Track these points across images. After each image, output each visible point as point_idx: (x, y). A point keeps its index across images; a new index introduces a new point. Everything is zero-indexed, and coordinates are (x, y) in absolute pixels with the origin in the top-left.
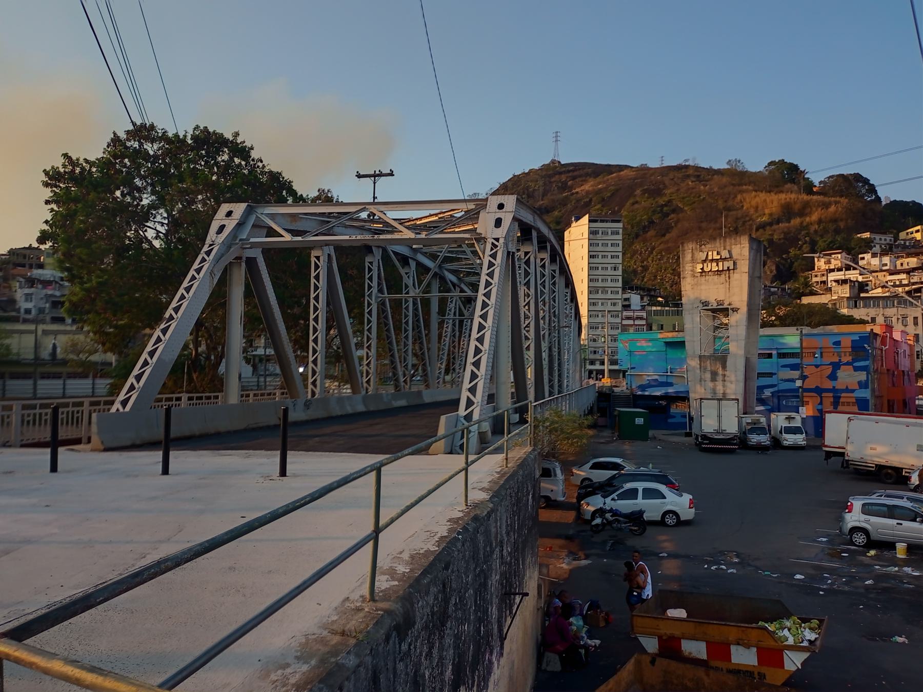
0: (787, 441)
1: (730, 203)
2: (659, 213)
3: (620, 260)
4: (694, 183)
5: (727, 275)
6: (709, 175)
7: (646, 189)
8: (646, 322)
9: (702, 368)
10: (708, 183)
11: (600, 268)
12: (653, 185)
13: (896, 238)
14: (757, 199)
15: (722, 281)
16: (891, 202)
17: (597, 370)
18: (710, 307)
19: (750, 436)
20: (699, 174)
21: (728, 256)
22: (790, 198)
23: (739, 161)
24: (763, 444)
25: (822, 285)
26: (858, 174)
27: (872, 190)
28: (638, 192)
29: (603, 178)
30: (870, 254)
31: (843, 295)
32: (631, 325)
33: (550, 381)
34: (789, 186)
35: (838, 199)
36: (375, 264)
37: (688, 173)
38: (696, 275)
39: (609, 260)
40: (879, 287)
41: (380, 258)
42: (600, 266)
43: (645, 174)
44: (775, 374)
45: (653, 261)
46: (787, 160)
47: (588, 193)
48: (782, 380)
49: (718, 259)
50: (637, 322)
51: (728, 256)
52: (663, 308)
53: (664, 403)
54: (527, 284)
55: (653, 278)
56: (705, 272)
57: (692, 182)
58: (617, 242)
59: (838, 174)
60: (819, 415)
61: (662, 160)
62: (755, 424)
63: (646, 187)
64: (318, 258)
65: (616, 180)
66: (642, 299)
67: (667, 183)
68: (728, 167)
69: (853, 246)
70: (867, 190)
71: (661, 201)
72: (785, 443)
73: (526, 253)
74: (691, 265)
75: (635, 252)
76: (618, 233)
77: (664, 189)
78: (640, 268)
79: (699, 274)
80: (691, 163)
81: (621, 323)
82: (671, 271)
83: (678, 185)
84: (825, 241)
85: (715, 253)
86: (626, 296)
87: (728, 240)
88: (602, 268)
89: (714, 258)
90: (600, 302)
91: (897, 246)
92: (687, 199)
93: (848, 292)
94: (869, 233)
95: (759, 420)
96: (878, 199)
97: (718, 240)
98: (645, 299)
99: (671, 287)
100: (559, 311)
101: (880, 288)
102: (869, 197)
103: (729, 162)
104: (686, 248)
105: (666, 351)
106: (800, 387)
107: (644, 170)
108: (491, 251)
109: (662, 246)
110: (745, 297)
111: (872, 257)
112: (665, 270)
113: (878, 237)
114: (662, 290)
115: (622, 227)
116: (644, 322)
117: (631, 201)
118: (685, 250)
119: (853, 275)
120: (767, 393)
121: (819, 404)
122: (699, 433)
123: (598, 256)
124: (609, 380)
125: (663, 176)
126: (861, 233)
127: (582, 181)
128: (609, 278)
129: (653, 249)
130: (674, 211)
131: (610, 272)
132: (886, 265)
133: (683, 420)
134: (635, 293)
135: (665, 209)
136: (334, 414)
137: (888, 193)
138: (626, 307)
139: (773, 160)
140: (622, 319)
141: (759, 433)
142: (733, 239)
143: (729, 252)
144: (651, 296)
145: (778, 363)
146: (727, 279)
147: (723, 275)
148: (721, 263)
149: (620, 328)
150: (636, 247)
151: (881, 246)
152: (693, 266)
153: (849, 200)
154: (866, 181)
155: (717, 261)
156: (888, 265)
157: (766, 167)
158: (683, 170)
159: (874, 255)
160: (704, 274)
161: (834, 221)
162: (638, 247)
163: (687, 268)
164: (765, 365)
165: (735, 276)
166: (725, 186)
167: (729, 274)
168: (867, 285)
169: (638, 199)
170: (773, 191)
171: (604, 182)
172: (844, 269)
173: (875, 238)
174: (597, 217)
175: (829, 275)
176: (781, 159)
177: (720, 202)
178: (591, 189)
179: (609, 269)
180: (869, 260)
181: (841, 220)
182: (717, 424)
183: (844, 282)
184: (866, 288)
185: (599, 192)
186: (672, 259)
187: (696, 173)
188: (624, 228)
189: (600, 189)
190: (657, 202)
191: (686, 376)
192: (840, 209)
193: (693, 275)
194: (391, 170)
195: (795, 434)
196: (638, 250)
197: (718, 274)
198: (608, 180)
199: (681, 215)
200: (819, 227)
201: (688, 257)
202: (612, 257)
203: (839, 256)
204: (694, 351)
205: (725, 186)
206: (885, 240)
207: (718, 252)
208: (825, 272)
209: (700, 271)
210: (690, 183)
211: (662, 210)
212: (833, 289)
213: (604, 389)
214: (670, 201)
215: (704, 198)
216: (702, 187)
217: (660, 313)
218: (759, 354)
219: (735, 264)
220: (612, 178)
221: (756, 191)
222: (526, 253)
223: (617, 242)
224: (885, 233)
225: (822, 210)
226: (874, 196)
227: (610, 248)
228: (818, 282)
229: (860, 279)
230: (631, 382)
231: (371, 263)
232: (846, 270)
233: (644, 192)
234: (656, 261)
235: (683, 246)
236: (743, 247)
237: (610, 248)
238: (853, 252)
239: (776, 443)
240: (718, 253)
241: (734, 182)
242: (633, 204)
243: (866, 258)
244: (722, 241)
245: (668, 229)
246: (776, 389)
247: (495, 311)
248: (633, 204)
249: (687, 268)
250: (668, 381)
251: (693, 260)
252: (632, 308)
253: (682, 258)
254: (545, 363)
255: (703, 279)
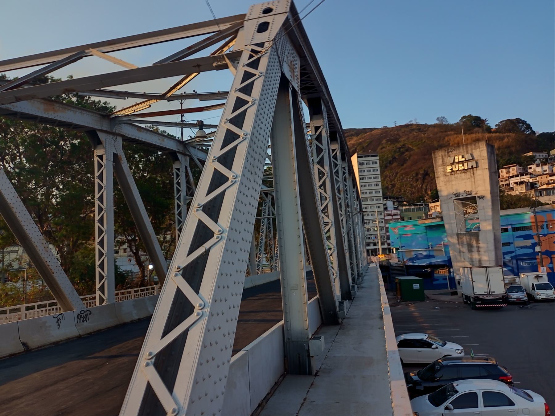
0: (540, 295)
1: (441, 143)
2: (398, 152)
3: (379, 180)
4: (417, 133)
5: (472, 172)
6: (426, 128)
7: (389, 139)
8: (400, 216)
9: (460, 243)
10: (426, 132)
11: (367, 186)
12: (393, 137)
13: (549, 155)
14: (458, 139)
15: (468, 177)
16: (540, 134)
17: (372, 249)
18: (461, 197)
19: (511, 294)
20: (419, 128)
21: (471, 158)
22: (479, 136)
23: (444, 117)
24: (521, 299)
25: (506, 186)
26: (518, 118)
27: (529, 127)
28: (384, 141)
29: (362, 135)
30: (535, 165)
31: (521, 191)
32: (391, 220)
33: (351, 263)
34: (476, 129)
35: (508, 134)
36: (183, 170)
37: (413, 128)
38: (447, 174)
39: (372, 180)
40: (544, 185)
41: (188, 165)
42: (367, 184)
43: (387, 131)
44: (512, 243)
45: (397, 181)
46: (474, 115)
47: (354, 145)
48: (518, 247)
49: (463, 161)
50: (394, 217)
51: (471, 158)
52: (410, 207)
53: (429, 270)
54: (321, 163)
55: (399, 191)
56: (454, 171)
57: (416, 132)
58: (377, 168)
59: (506, 119)
60: (551, 272)
61: (395, 124)
62: (511, 284)
63: (388, 138)
64: (101, 157)
65: (370, 136)
66: (394, 204)
67: (401, 134)
68: (437, 122)
69: (522, 161)
70: (525, 128)
71: (399, 145)
72: (539, 297)
73: (317, 129)
74: (442, 167)
75: (386, 176)
76: (376, 163)
77: (399, 138)
78: (390, 186)
79: (450, 174)
80: (414, 122)
81: (384, 218)
82: (410, 186)
83: (408, 135)
84: (504, 160)
85: (460, 157)
86: (385, 202)
87: (469, 146)
88: (369, 185)
89: (460, 160)
90: (369, 206)
91: (551, 159)
92: (415, 142)
93: (525, 189)
94: (532, 153)
95: (514, 280)
96: (533, 133)
97: (461, 148)
98: (396, 204)
99: (411, 195)
100: (351, 202)
101: (545, 185)
102: (527, 132)
103: (438, 119)
104: (437, 155)
105: (426, 232)
106: (539, 252)
107: (385, 130)
108: (249, 59)
109: (403, 171)
110: (488, 187)
111: (536, 167)
112: (406, 185)
113: (537, 154)
114: (405, 198)
115: (378, 159)
116: (399, 217)
117: (380, 147)
118: (436, 157)
119: (526, 178)
120: (508, 258)
121: (550, 264)
122: (472, 295)
123: (365, 178)
124: (383, 256)
125: (398, 131)
126: (526, 153)
127: (349, 139)
128: (374, 191)
129: (397, 173)
130: (407, 150)
131: (374, 187)
132: (546, 171)
133: (444, 282)
134: (389, 201)
135: (402, 149)
136: (127, 320)
137: (539, 128)
138: (386, 209)
139: (465, 115)
140: (385, 216)
141: (517, 291)
142: (473, 145)
143: (472, 155)
144: (399, 202)
145: (513, 235)
146: (472, 175)
147: (468, 173)
148: (466, 164)
149: (384, 222)
150: (386, 173)
151: (540, 160)
152: (444, 168)
153: (516, 134)
154: (524, 122)
155: (462, 162)
156: (548, 170)
157: (460, 120)
158: (410, 127)
159: (538, 165)
160: (453, 173)
161: (508, 147)
162: (387, 173)
163: (439, 171)
164: (504, 237)
165: (478, 172)
166: (437, 133)
167: (473, 171)
168: (536, 184)
169: (384, 145)
170: (467, 133)
171: (363, 138)
172: (519, 175)
173: (536, 155)
174: (362, 154)
175: (510, 180)
176: (469, 114)
177: (435, 143)
178: (355, 142)
179: (373, 185)
180: (533, 168)
181: (513, 146)
182: (487, 287)
183: (521, 183)
184: (535, 186)
185: (360, 144)
186: (410, 178)
187: (418, 128)
188: (380, 160)
189: (361, 142)
190: (396, 146)
191: (443, 250)
192: (511, 140)
193: (445, 174)
194: (194, 91)
195: (546, 290)
196: (387, 175)
197: (464, 172)
198: (365, 137)
199: (412, 152)
200: (499, 152)
201: (440, 162)
202: (374, 178)
203: (515, 168)
204: (452, 231)
205: (437, 133)
206: (543, 156)
207: (462, 156)
208: (508, 178)
209: (451, 171)
210: (415, 133)
211: (399, 151)
212: (514, 188)
213: (384, 263)
214: (404, 145)
215: (425, 141)
216: (423, 135)
217: (409, 210)
218: (501, 229)
219: (477, 163)
220: (367, 135)
221: (457, 134)
222: (317, 129)
223: (377, 168)
224: (542, 152)
225: (499, 141)
226: (530, 131)
227: (372, 173)
228: (503, 185)
229: (531, 180)
230: (403, 256)
231: (178, 169)
232: (521, 176)
233: (388, 141)
234: (399, 181)
235: (434, 154)
236: (482, 150)
237: (372, 173)
238: (523, 165)
239: (531, 298)
240: (463, 157)
241: (442, 130)
242: (382, 149)
243: (533, 168)
244: (465, 148)
245: (405, 161)
246: (513, 254)
247: (250, 146)
248: (382, 149)
249: (439, 170)
250: (430, 254)
251: (444, 164)
252: (388, 209)
253: (435, 163)
254: (346, 247)
255: (453, 177)
